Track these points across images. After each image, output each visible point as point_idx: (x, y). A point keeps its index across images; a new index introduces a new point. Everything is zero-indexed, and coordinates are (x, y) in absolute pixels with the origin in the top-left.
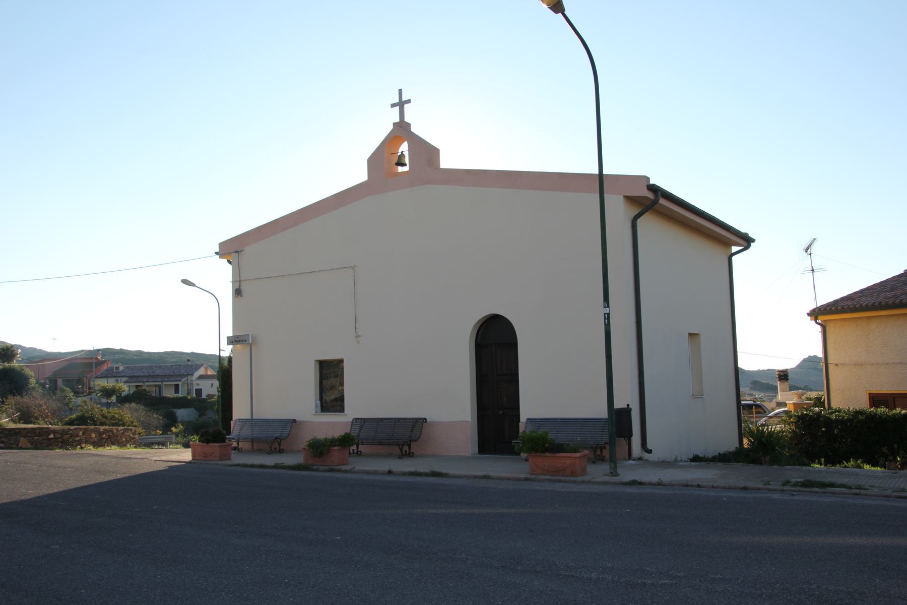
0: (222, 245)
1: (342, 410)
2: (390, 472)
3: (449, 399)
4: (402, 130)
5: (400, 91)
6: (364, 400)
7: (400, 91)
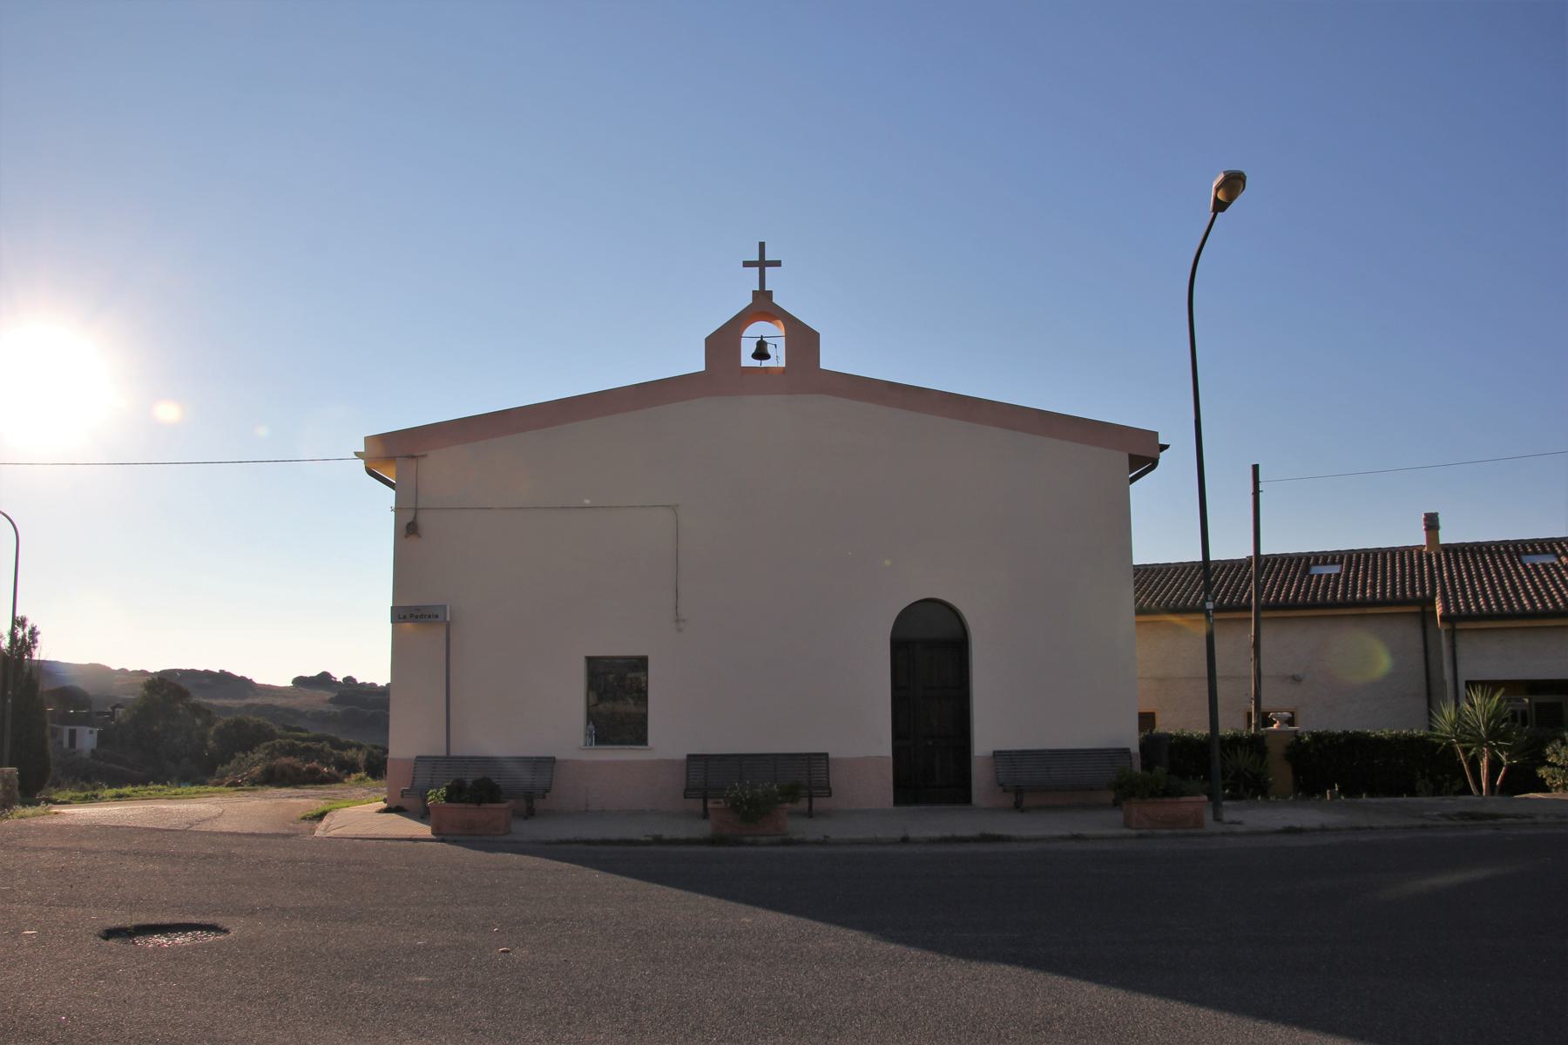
1: (641, 739)
2: (905, 840)
4: (763, 306)
5: (762, 245)
6: (678, 729)
7: (762, 245)
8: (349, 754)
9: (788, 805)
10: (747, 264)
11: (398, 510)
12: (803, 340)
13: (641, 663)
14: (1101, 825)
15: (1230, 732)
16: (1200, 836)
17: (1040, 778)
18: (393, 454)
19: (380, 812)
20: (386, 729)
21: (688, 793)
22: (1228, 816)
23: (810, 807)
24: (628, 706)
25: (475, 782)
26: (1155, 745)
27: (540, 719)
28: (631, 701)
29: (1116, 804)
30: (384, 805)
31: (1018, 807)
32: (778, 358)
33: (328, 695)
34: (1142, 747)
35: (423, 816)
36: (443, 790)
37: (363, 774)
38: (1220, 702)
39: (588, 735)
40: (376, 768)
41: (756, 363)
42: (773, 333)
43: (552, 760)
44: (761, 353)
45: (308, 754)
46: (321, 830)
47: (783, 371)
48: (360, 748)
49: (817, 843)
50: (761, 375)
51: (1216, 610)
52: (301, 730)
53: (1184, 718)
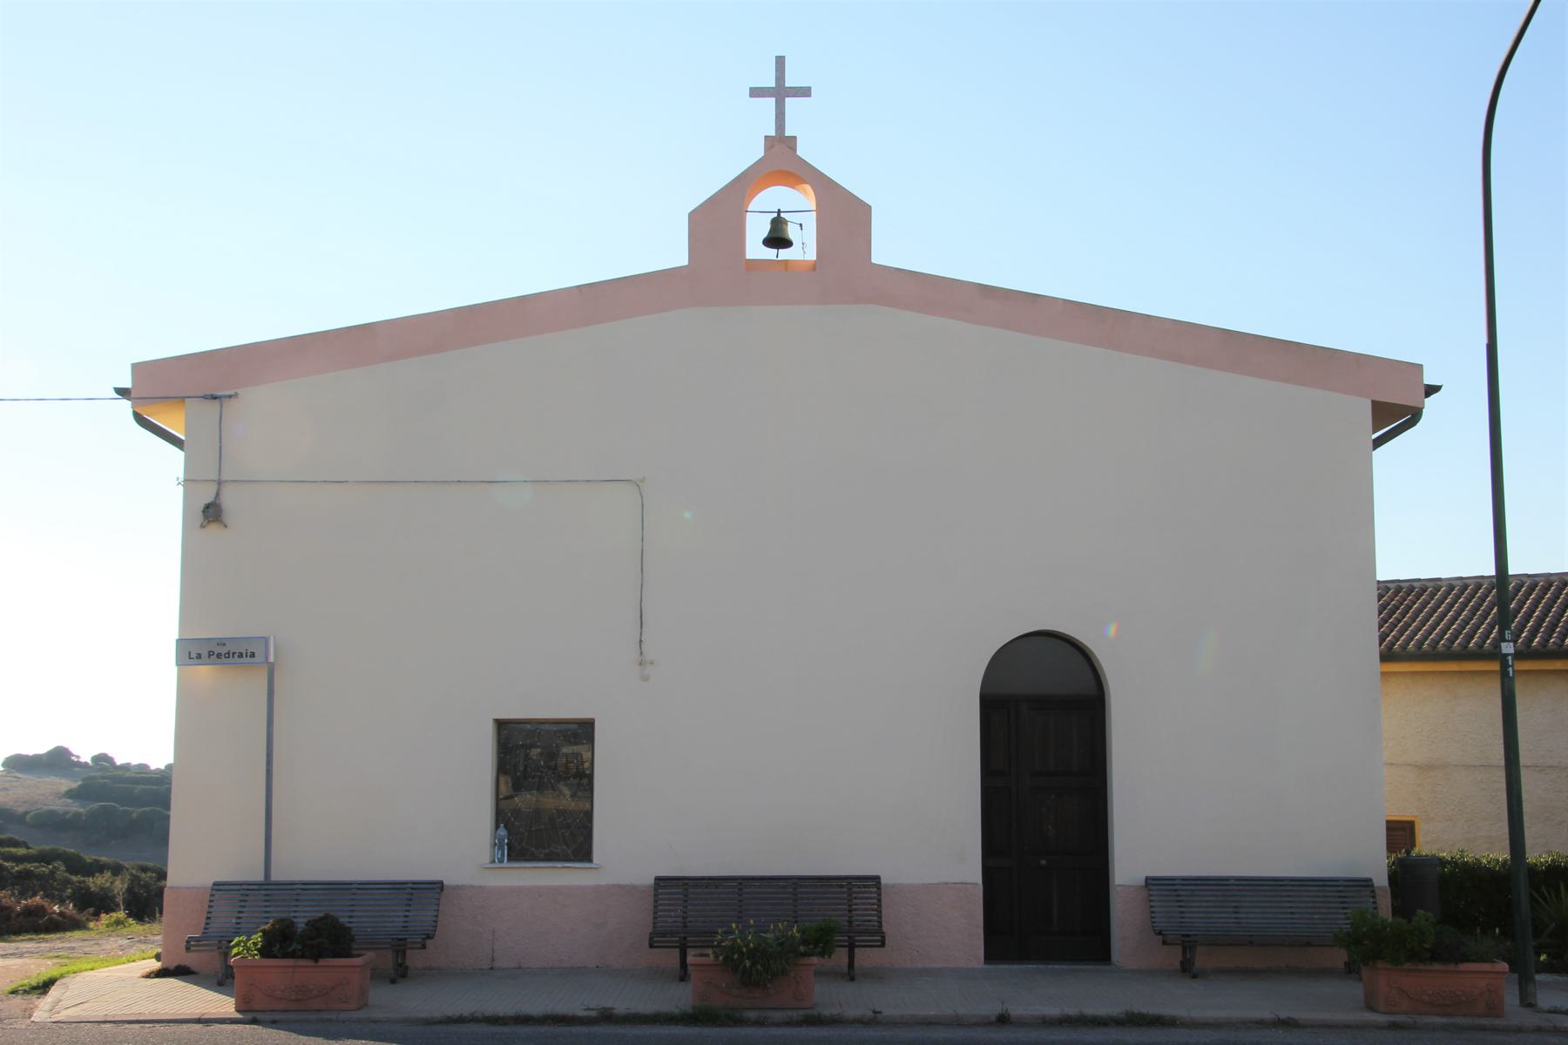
0: (139, 369)
1: (581, 850)
2: (1003, 1020)
3: (918, 826)
4: (781, 161)
5: (780, 62)
6: (648, 827)
7: (780, 62)
8: (97, 882)
9: (815, 960)
10: (756, 92)
11: (189, 482)
12: (845, 216)
13: (583, 731)
14: (1331, 1001)
15: (1545, 858)
16: (1495, 1030)
17: (1226, 925)
18: (172, 392)
19: (148, 976)
20: (164, 840)
21: (656, 939)
22: (1545, 999)
23: (851, 964)
24: (562, 799)
25: (312, 924)
26: (1411, 874)
27: (426, 820)
28: (567, 792)
29: (1351, 970)
30: (156, 965)
31: (1187, 969)
32: (804, 246)
33: (66, 784)
34: (1393, 878)
35: (222, 980)
36: (257, 938)
37: (121, 915)
38: (1527, 808)
39: (497, 845)
40: (144, 904)
41: (770, 254)
42: (796, 204)
43: (438, 887)
44: (777, 240)
45: (25, 883)
46: (43, 1009)
47: (813, 267)
48: (117, 870)
49: (860, 1021)
50: (778, 271)
51: (1518, 655)
52: (16, 844)
53: (1464, 831)
